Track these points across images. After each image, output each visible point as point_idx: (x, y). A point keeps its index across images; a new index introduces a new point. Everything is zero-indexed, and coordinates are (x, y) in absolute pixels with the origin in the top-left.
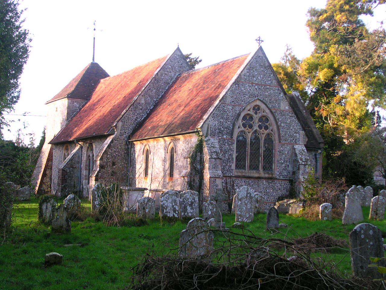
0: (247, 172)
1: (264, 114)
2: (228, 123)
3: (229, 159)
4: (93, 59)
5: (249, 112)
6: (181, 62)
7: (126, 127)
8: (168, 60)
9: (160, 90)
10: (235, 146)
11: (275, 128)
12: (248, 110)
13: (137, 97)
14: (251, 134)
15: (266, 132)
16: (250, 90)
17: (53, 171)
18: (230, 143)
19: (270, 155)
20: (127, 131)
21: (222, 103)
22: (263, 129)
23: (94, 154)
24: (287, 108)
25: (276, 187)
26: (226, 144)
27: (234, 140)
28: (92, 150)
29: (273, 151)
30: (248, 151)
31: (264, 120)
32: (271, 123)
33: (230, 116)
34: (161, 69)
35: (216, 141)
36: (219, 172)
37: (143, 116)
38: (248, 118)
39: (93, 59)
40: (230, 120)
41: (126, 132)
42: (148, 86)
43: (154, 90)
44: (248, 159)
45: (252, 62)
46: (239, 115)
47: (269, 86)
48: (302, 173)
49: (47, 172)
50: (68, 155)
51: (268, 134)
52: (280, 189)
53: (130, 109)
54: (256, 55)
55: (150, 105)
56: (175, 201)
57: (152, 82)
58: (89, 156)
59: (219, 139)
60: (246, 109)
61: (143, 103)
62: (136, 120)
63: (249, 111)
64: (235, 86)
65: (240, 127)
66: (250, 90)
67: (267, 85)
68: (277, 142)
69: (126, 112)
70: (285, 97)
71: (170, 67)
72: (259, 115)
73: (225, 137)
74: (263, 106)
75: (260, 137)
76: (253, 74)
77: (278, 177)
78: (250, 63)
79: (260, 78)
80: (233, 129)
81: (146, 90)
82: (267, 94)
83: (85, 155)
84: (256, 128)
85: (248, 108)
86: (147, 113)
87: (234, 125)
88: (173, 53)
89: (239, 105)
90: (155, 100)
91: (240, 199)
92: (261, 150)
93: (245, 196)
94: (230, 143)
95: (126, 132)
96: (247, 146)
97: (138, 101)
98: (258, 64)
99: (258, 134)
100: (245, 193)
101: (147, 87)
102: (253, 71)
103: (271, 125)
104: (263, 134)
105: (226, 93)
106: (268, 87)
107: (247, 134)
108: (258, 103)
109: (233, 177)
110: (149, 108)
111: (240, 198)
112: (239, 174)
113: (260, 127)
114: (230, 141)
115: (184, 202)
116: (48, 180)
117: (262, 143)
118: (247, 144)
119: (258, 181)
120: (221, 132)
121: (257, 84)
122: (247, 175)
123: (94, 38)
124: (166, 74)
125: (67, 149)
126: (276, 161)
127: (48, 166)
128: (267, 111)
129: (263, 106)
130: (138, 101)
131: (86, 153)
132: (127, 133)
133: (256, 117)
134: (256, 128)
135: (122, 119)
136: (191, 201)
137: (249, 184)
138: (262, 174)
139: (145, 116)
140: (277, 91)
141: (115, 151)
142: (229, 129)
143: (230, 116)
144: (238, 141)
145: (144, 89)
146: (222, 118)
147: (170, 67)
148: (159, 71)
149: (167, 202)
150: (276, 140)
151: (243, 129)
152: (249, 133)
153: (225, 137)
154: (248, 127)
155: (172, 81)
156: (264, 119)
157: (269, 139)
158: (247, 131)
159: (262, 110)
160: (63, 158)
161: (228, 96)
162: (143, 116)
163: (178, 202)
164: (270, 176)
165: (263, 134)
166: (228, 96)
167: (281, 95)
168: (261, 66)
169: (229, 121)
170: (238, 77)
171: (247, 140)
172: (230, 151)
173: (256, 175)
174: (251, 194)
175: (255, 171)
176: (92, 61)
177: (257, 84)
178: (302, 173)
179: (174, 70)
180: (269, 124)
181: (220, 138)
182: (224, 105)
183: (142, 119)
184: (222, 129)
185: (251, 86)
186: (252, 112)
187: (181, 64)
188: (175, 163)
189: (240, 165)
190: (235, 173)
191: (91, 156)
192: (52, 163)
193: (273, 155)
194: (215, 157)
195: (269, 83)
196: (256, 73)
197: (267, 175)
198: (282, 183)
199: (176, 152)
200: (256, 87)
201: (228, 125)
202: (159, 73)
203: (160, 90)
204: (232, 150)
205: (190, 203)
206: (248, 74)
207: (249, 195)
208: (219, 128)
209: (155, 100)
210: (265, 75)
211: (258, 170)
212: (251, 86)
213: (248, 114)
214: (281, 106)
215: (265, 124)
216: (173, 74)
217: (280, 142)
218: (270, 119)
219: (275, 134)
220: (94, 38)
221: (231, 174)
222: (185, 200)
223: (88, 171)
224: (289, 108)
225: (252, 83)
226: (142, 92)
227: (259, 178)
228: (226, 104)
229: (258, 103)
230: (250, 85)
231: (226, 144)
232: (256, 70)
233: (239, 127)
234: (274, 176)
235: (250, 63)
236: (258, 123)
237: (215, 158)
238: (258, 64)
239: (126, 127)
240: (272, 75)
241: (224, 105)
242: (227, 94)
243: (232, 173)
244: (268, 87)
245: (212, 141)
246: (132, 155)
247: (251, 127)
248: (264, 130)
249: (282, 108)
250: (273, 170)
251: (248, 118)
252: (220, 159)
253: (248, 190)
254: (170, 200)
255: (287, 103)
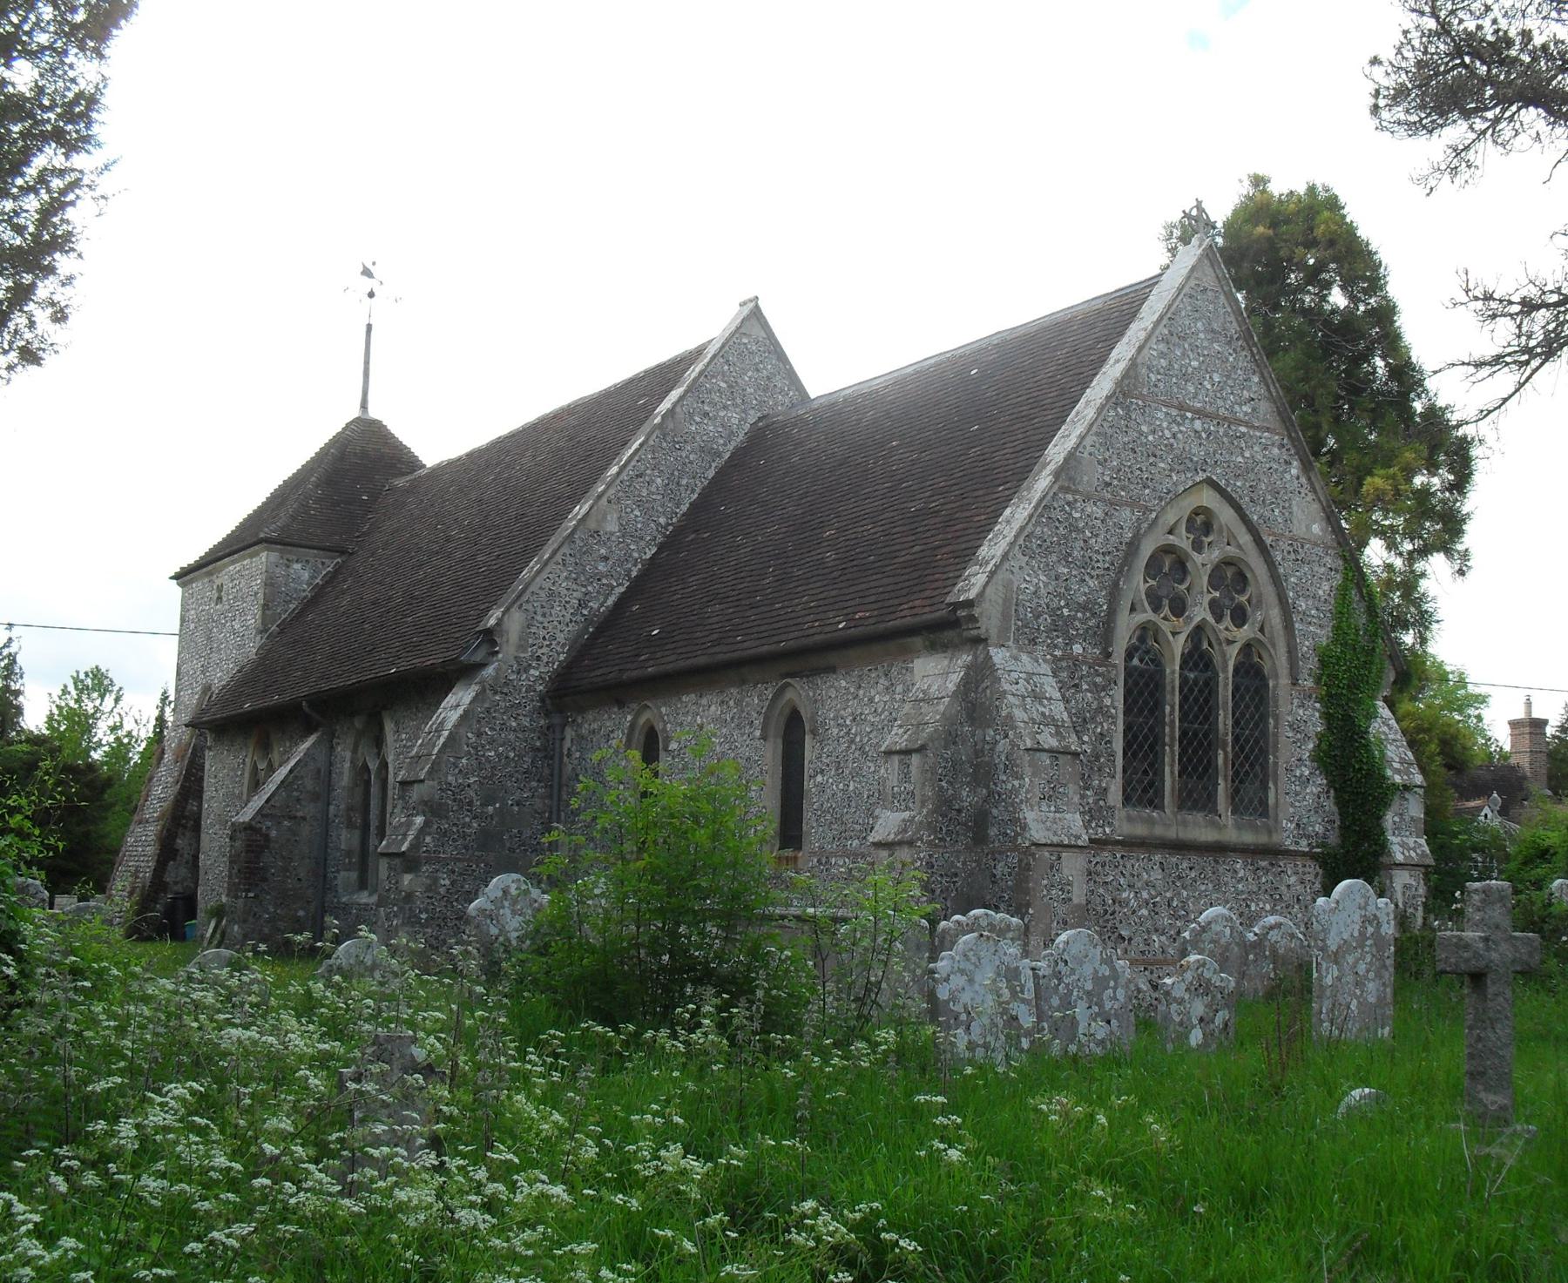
0: (1169, 822)
1: (1231, 550)
2: (1091, 583)
3: (1097, 758)
4: (364, 405)
5: (1171, 537)
6: (765, 368)
7: (542, 633)
8: (714, 356)
9: (684, 482)
10: (1119, 692)
11: (1275, 614)
12: (1166, 529)
13: (586, 507)
14: (1182, 638)
15: (1245, 633)
16: (1174, 436)
17: (203, 836)
18: (1098, 680)
19: (1257, 742)
20: (545, 650)
21: (1061, 488)
22: (1227, 621)
23: (390, 759)
24: (1316, 528)
25: (1283, 888)
26: (1085, 687)
27: (1115, 666)
28: (379, 742)
29: (1267, 723)
30: (1173, 722)
31: (1231, 576)
32: (1260, 595)
33: (1097, 552)
34: (686, 392)
35: (1045, 668)
36: (1068, 816)
37: (613, 588)
38: (1166, 569)
39: (364, 405)
40: (1097, 572)
41: (538, 658)
42: (633, 463)
43: (659, 480)
44: (1173, 760)
45: (1178, 311)
46: (1133, 547)
47: (1247, 424)
48: (1395, 823)
49: (179, 841)
50: (271, 769)
51: (1247, 647)
52: (1298, 900)
53: (559, 557)
54: (1192, 283)
55: (642, 543)
56: (1012, 975)
57: (651, 442)
58: (366, 768)
59: (1056, 659)
60: (1161, 521)
61: (612, 534)
62: (582, 604)
63: (1170, 532)
64: (1112, 413)
65: (1138, 607)
66: (1174, 436)
67: (1240, 422)
68: (1284, 680)
69: (539, 572)
70: (1309, 479)
71: (723, 385)
72: (1214, 555)
73: (1077, 649)
74: (1226, 515)
75: (1217, 660)
76: (1182, 366)
77: (1289, 843)
78: (1169, 315)
79: (1209, 387)
80: (1112, 612)
81: (624, 476)
82: (1240, 459)
83: (347, 765)
84: (1200, 612)
85: (1170, 518)
86: (628, 575)
87: (1114, 593)
88: (738, 328)
89: (1133, 503)
90: (662, 520)
91: (1336, 954)
92: (1221, 718)
93: (1356, 934)
94: (1098, 680)
95: (538, 658)
96: (1168, 697)
97: (592, 524)
98: (1199, 324)
99: (1210, 644)
100: (1357, 918)
101: (630, 467)
102: (1183, 354)
103: (1260, 602)
104: (1230, 642)
105: (1082, 438)
106: (1243, 429)
107: (1169, 641)
108: (1208, 498)
109: (1117, 842)
110: (636, 555)
111: (1334, 948)
112: (1140, 830)
113: (1215, 607)
114: (1101, 670)
115: (1060, 980)
116: (183, 872)
117: (1226, 685)
118: (1168, 688)
119: (1217, 862)
120: (1060, 626)
121: (1200, 414)
122: (1172, 833)
123: (369, 327)
124: (706, 414)
125: (265, 747)
126: (1281, 771)
127: (185, 817)
128: (1245, 538)
129: (1226, 515)
130: (592, 524)
131: (348, 755)
132: (545, 659)
133: (1203, 561)
134: (1200, 612)
135: (525, 598)
136: (1096, 972)
137: (1179, 877)
138: (1229, 828)
139: (622, 589)
140: (1276, 451)
141: (492, 741)
142: (1094, 615)
143: (1097, 552)
144: (1129, 672)
145: (618, 474)
146: (1066, 558)
147: (723, 385)
148: (681, 398)
149: (971, 981)
150: (1280, 672)
151: (1147, 615)
152: (1174, 634)
153: (1077, 649)
154: (1166, 610)
155: (733, 444)
156: (1230, 572)
157: (1252, 666)
158: (1166, 627)
159: (1221, 531)
160: (246, 781)
161: (1086, 455)
162: (613, 588)
163: (1030, 985)
164: (1263, 839)
165: (1230, 642)
166: (1086, 455)
167: (1294, 472)
168: (1213, 331)
169: (1093, 573)
170: (1126, 375)
171: (1168, 671)
172: (1099, 718)
173: (1206, 835)
174: (1379, 925)
175: (1200, 816)
176: (354, 412)
177: (1200, 414)
178: (1395, 823)
179: (739, 401)
180: (1249, 601)
181: (1058, 653)
182: (1070, 497)
183: (610, 602)
184: (1066, 612)
185: (1178, 419)
186: (1183, 541)
187: (768, 378)
188: (809, 785)
189: (1141, 791)
190: (1124, 824)
191: (373, 765)
192: (200, 806)
193: (1267, 743)
194: (1053, 743)
195: (1246, 414)
196: (1195, 364)
197: (1248, 838)
198: (1307, 870)
199: (814, 733)
200: (1198, 425)
201: (1092, 591)
202: (678, 409)
203: (684, 482)
204: (1107, 715)
205: (1089, 986)
206: (1163, 362)
207: (1370, 930)
208: (1054, 605)
209: (662, 520)
210: (1228, 377)
211: (1214, 811)
212: (1178, 419)
213: (1168, 549)
214: (1295, 522)
215: (1233, 599)
216: (734, 417)
217: (1295, 683)
218: (1255, 576)
219: (1274, 645)
220: (369, 327)
221: (1108, 830)
222: (1061, 965)
223: (357, 833)
224: (1322, 530)
225: (1182, 407)
226: (609, 486)
227: (1219, 850)
228: (1076, 492)
229: (1208, 498)
230: (1174, 412)
231: (1085, 687)
232: (1194, 348)
233: (1133, 609)
234: (1276, 838)
235: (1169, 316)
236: (1209, 592)
237: (1050, 751)
238: (1199, 324)
239: (542, 633)
240: (1256, 379)
241: (1070, 497)
242: (1080, 449)
243: (1110, 824)
244: (1243, 429)
245: (1029, 668)
246: (569, 755)
247: (1179, 608)
248: (1232, 627)
249: (1299, 530)
250: (1271, 812)
251: (1166, 569)
252: (1076, 755)
253: (1367, 904)
254: (986, 976)
255: (1316, 506)
